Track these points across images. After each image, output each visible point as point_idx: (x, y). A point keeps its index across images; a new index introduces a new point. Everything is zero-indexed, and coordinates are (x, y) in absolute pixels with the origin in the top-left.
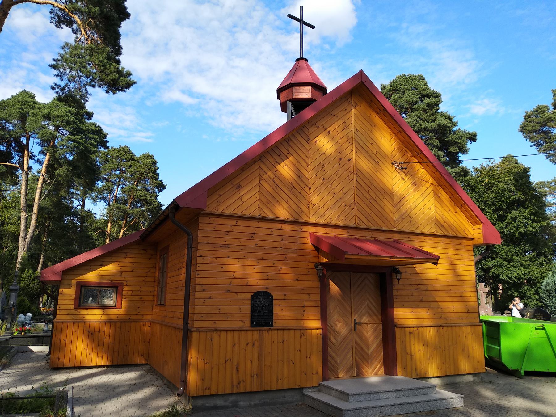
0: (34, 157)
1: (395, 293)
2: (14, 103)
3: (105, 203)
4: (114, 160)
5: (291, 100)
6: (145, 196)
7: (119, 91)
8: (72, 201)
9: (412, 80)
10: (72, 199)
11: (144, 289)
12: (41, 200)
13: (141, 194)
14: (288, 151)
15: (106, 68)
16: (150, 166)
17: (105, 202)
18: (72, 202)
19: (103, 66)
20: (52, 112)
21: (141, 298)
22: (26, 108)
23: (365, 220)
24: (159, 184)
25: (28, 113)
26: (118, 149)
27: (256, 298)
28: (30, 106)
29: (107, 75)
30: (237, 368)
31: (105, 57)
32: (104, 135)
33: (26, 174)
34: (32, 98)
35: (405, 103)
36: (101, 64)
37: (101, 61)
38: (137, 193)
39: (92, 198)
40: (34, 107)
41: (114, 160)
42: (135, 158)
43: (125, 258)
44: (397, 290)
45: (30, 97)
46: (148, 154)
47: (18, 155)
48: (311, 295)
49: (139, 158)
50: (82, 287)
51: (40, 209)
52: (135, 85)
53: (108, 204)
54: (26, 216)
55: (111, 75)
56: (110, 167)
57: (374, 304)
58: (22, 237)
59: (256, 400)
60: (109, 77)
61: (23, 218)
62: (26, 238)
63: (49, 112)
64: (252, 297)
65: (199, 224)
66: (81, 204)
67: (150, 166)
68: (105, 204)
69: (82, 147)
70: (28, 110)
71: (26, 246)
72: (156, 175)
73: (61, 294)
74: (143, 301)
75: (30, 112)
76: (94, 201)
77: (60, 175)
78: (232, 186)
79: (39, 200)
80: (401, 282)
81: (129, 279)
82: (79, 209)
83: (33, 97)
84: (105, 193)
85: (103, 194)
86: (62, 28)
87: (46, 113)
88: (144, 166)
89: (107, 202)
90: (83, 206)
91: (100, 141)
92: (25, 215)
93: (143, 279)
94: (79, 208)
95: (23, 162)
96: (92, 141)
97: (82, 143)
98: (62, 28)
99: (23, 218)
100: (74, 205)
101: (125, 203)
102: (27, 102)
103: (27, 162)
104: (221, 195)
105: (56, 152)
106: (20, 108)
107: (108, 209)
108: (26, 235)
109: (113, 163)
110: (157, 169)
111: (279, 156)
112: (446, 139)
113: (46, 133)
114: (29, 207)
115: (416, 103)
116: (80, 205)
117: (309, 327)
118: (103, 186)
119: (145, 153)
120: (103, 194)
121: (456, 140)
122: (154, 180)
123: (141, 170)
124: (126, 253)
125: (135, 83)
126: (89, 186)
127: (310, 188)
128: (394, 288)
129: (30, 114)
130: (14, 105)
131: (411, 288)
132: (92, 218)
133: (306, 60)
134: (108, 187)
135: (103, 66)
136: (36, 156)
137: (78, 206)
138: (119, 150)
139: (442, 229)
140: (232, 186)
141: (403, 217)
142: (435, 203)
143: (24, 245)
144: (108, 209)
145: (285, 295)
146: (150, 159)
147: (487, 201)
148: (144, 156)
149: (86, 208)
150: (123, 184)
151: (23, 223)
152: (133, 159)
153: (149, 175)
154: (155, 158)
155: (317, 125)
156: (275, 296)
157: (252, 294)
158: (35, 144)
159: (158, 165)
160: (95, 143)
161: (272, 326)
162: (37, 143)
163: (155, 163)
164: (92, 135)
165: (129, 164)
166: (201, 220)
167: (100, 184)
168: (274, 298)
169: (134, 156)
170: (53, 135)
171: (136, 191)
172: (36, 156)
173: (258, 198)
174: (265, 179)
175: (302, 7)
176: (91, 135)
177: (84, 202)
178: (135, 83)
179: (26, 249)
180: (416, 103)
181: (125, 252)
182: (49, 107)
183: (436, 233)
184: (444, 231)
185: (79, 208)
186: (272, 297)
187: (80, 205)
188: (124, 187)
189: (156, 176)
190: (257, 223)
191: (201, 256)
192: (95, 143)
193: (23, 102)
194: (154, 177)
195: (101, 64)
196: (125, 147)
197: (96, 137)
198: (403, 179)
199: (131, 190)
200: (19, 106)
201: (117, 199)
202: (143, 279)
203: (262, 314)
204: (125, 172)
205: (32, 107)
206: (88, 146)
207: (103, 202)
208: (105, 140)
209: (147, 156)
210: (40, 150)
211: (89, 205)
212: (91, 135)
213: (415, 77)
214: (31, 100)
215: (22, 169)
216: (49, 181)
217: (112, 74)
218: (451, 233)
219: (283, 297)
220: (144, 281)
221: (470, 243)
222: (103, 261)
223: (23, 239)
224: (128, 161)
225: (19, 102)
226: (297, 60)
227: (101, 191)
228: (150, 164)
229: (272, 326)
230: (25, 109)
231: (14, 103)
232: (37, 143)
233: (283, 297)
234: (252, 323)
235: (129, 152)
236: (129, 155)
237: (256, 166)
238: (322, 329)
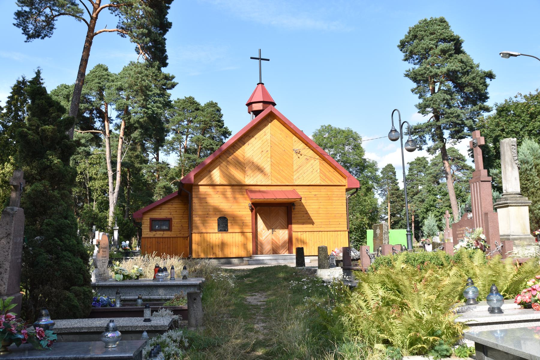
1: (293, 216)
2: (93, 78)
3: (176, 154)
4: (180, 112)
5: (252, 111)
6: (211, 145)
9: (432, 24)
11: (183, 221)
17: (176, 153)
18: (148, 155)
19: (155, 76)
20: (123, 84)
22: (102, 81)
23: (276, 181)
24: (223, 132)
25: (105, 86)
26: (183, 100)
29: (159, 81)
32: (168, 96)
36: (154, 74)
37: (154, 73)
38: (203, 143)
40: (109, 79)
41: (180, 112)
42: (200, 108)
45: (104, 70)
46: (212, 102)
47: (100, 121)
51: (123, 164)
66: (156, 157)
71: (115, 199)
76: (168, 153)
79: (121, 159)
81: (175, 216)
82: (155, 162)
83: (106, 70)
86: (125, 37)
89: (178, 153)
90: (157, 159)
93: (182, 216)
96: (158, 104)
97: (150, 108)
98: (125, 37)
101: (195, 152)
102: (103, 76)
106: (97, 83)
108: (114, 189)
112: (458, 82)
114: (114, 164)
115: (431, 49)
116: (155, 158)
118: (173, 138)
121: (470, 81)
122: (218, 128)
125: (178, 83)
126: (159, 143)
127: (245, 168)
130: (93, 80)
131: (302, 213)
133: (263, 84)
135: (155, 76)
138: (184, 101)
143: (113, 199)
147: (531, 131)
149: (160, 160)
152: (197, 109)
154: (219, 105)
156: (228, 219)
158: (112, 110)
159: (222, 112)
162: (113, 109)
163: (219, 110)
165: (194, 114)
166: (193, 187)
167: (170, 137)
171: (203, 140)
176: (157, 99)
177: (158, 155)
178: (178, 83)
180: (431, 49)
183: (320, 184)
185: (154, 160)
187: (155, 158)
188: (193, 136)
189: (220, 123)
192: (161, 105)
194: (219, 125)
195: (154, 74)
196: (190, 98)
197: (161, 99)
200: (97, 81)
201: (187, 150)
202: (182, 216)
204: (191, 122)
207: (174, 153)
209: (212, 105)
211: (162, 157)
212: (157, 99)
213: (436, 20)
215: (105, 133)
221: (345, 188)
225: (96, 77)
226: (258, 84)
227: (171, 143)
229: (227, 231)
230: (102, 83)
231: (93, 78)
232: (113, 109)
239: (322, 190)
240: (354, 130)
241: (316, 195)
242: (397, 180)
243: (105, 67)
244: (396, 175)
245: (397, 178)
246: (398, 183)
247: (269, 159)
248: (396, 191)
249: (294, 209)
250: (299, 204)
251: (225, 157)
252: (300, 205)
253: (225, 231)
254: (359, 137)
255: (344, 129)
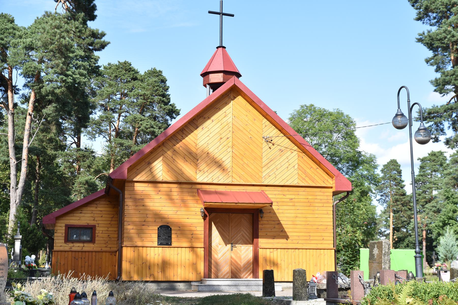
0: (18, 91)
1: (260, 226)
4: (112, 82)
5: (209, 84)
6: (152, 127)
7: (96, 51)
8: (65, 137)
10: (65, 135)
11: (110, 229)
12: (30, 144)
13: (147, 125)
14: (182, 137)
15: (82, 33)
16: (157, 86)
17: (104, 137)
19: (79, 32)
21: (109, 236)
22: (6, 37)
26: (116, 66)
27: (161, 229)
28: (9, 34)
29: (84, 39)
30: (149, 267)
31: (81, 22)
32: (95, 59)
33: (12, 114)
34: (11, 23)
35: (441, 5)
36: (78, 30)
37: (77, 28)
38: (141, 124)
39: (89, 133)
40: (15, 34)
41: (112, 82)
43: (96, 207)
44: (262, 224)
45: (9, 21)
46: (155, 69)
48: (197, 227)
49: (143, 77)
50: (69, 228)
51: (30, 151)
52: (109, 46)
53: (108, 139)
54: (15, 164)
55: (87, 39)
56: (107, 91)
57: (247, 234)
58: (13, 188)
59: (163, 285)
60: (85, 41)
61: (12, 165)
62: (17, 189)
63: (31, 42)
64: (158, 228)
65: (126, 187)
66: (76, 141)
67: (157, 86)
68: (105, 139)
69: (70, 80)
70: (8, 40)
71: (18, 198)
72: (164, 99)
73: (56, 233)
74: (110, 237)
75: (11, 42)
76: (93, 137)
77: (49, 115)
78: (145, 163)
79: (29, 143)
80: (263, 219)
82: (74, 148)
83: (12, 21)
84: (104, 126)
85: (101, 127)
87: (28, 43)
88: (150, 87)
89: (107, 136)
90: (78, 145)
91: (90, 68)
92: (14, 162)
93: (109, 222)
94: (73, 147)
95: (7, 97)
97: (70, 75)
99: (12, 165)
100: (68, 143)
101: (130, 136)
103: (12, 100)
104: (138, 169)
105: (43, 88)
107: (108, 147)
108: (17, 183)
109: (110, 85)
110: (167, 89)
111: (176, 141)
113: (30, 67)
114: (18, 149)
117: (195, 247)
118: (101, 117)
119: (150, 69)
120: (101, 127)
122: (162, 105)
123: (145, 94)
124: (97, 204)
125: (109, 43)
127: (198, 160)
128: (259, 223)
129: (11, 45)
132: (90, 159)
134: (107, 117)
135: (79, 32)
136: (21, 90)
137: (72, 144)
138: (118, 67)
139: (303, 181)
140: (145, 163)
141: (269, 175)
142: (299, 163)
143: (16, 197)
144: (108, 147)
145: (180, 228)
146: (157, 76)
148: (150, 73)
150: (126, 112)
151: (13, 171)
152: (135, 79)
153: (156, 98)
155: (204, 116)
157: (158, 227)
160: (85, 72)
161: (171, 245)
163: (164, 81)
164: (81, 62)
165: (130, 85)
166: (126, 184)
167: (96, 115)
168: (172, 229)
169: (137, 73)
170: (38, 69)
171: (141, 121)
172: (21, 90)
173: (162, 169)
174: (166, 157)
175: (222, 1)
176: (80, 63)
179: (18, 201)
181: (97, 203)
182: (31, 34)
183: (297, 185)
184: (305, 182)
185: (74, 146)
186: (171, 228)
187: (75, 142)
188: (128, 114)
190: (131, 184)
191: (127, 205)
192: (85, 72)
193: (2, 29)
194: (163, 101)
196: (125, 63)
197: (86, 64)
198: (270, 148)
199: (135, 120)
201: (119, 134)
202: (109, 222)
203: (164, 238)
204: (126, 95)
205: (12, 34)
206: (76, 78)
207: (101, 136)
208: (97, 65)
210: (25, 83)
212: (80, 63)
214: (10, 25)
216: (37, 121)
217: (88, 38)
218: (311, 184)
219: (178, 229)
220: (110, 224)
221: (331, 190)
222: (82, 210)
223: (14, 189)
224: (129, 81)
227: (98, 124)
228: (156, 84)
229: (171, 245)
230: (5, 39)
232: (20, 75)
233: (178, 229)
234: (158, 243)
235: (130, 69)
236: (130, 73)
237: (160, 149)
238: (204, 248)
239: (301, 193)
240: (346, 113)
241: (292, 199)
242: (403, 181)
243: (11, 18)
244: (402, 174)
245: (403, 178)
246: (404, 186)
247: (230, 149)
248: (402, 197)
249: (262, 217)
250: (269, 211)
251: (170, 144)
252: (270, 212)
253: (167, 244)
254: (352, 122)
255: (331, 110)
